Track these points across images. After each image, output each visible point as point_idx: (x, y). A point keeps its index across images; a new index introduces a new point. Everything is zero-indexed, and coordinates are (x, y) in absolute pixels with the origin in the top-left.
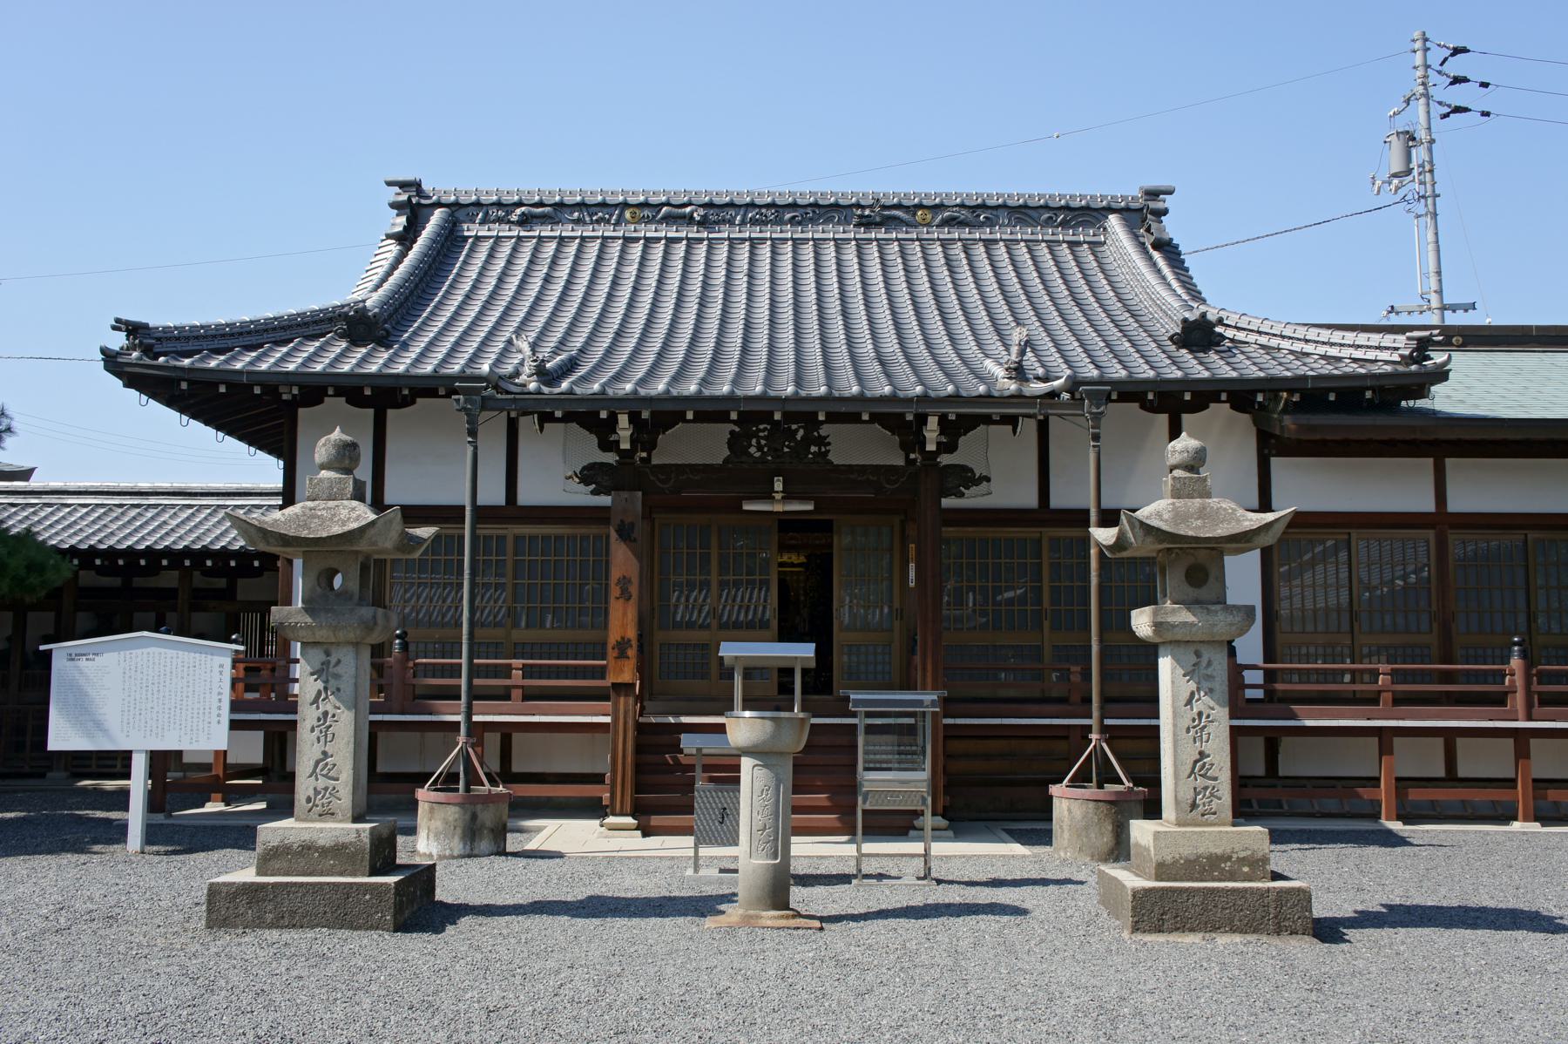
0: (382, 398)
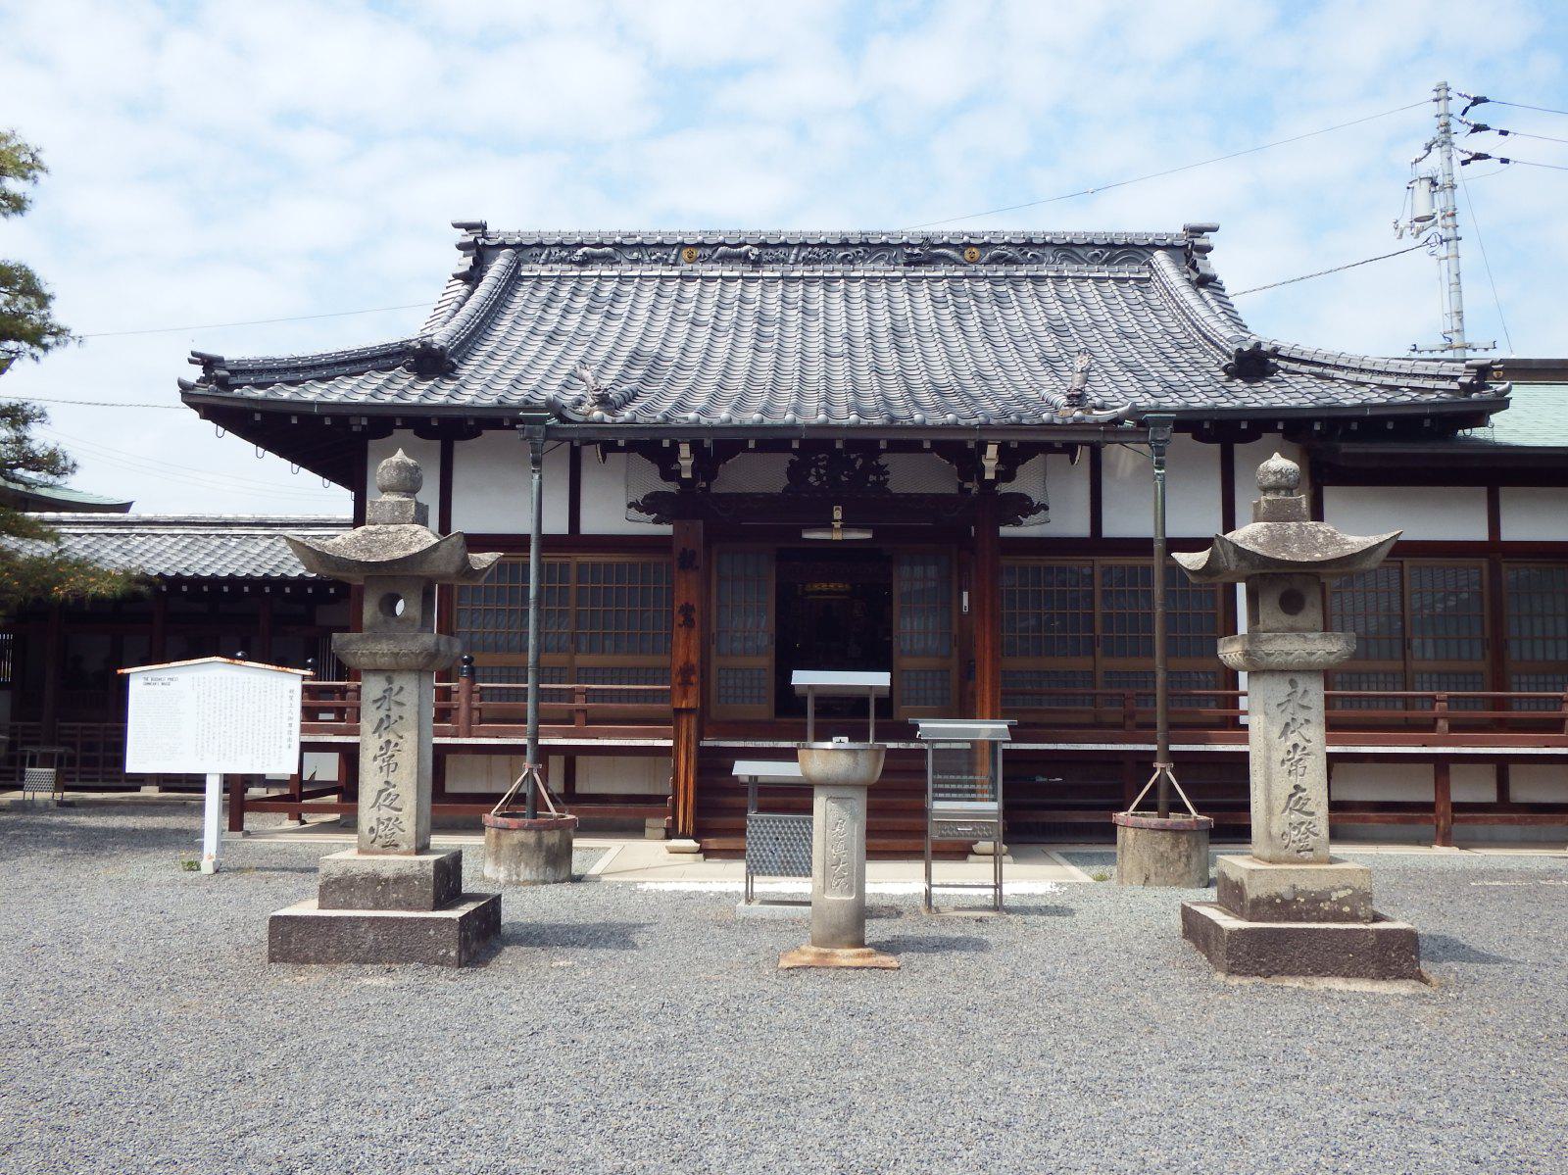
0: (450, 432)
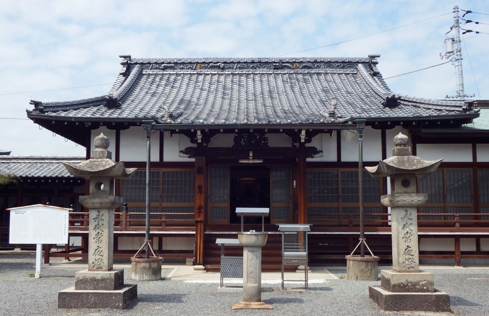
0: (119, 127)
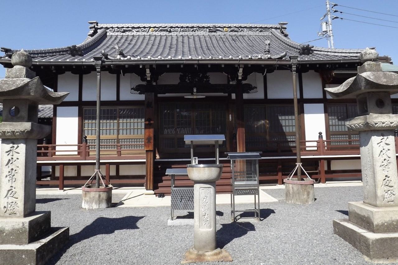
0: (82, 71)
